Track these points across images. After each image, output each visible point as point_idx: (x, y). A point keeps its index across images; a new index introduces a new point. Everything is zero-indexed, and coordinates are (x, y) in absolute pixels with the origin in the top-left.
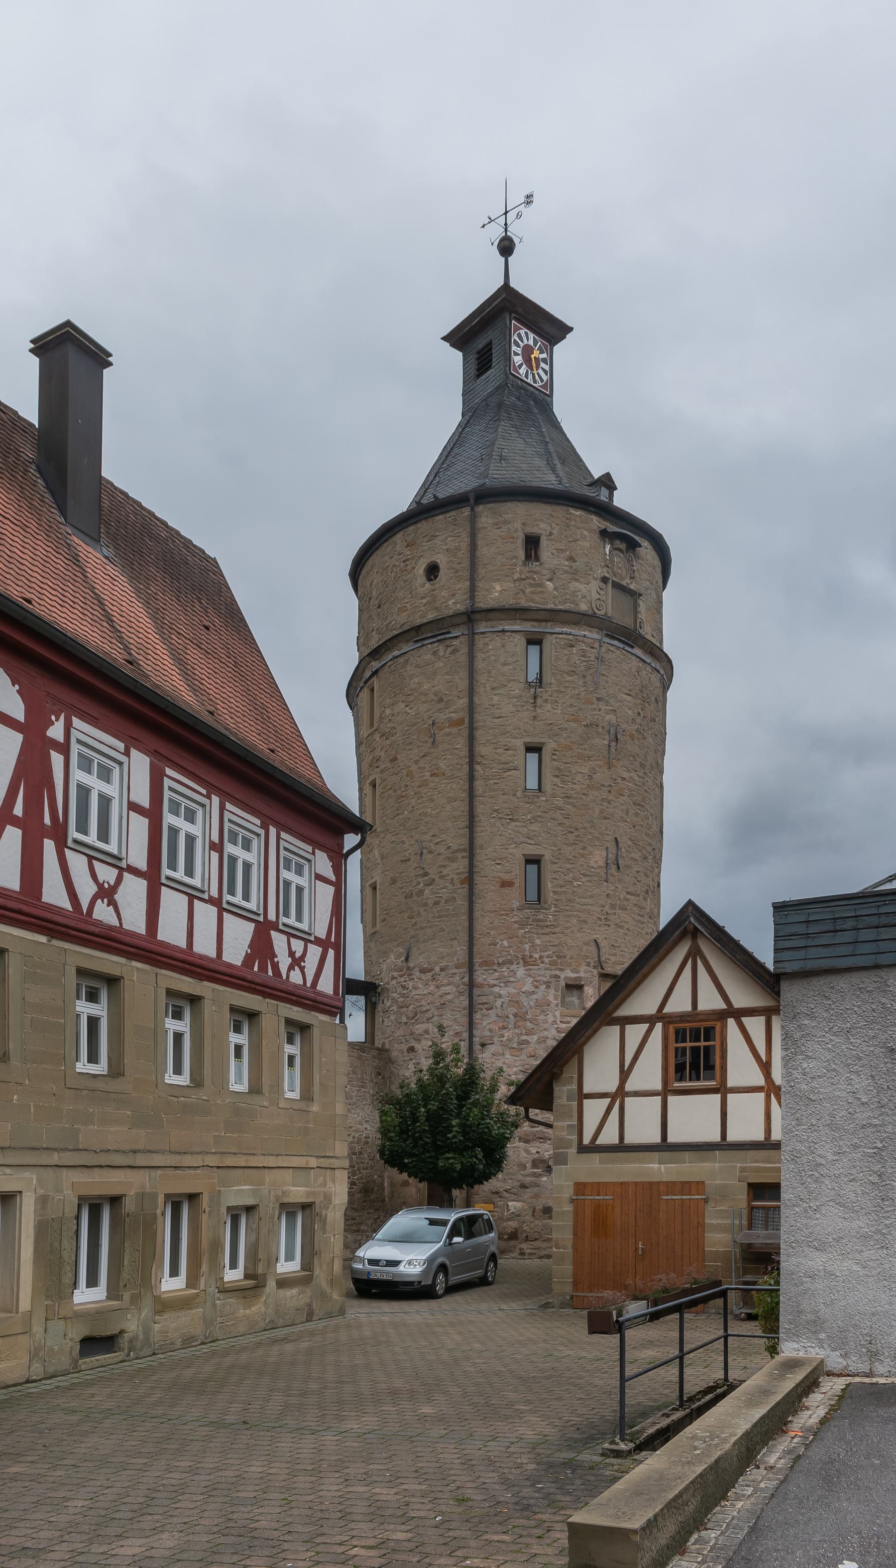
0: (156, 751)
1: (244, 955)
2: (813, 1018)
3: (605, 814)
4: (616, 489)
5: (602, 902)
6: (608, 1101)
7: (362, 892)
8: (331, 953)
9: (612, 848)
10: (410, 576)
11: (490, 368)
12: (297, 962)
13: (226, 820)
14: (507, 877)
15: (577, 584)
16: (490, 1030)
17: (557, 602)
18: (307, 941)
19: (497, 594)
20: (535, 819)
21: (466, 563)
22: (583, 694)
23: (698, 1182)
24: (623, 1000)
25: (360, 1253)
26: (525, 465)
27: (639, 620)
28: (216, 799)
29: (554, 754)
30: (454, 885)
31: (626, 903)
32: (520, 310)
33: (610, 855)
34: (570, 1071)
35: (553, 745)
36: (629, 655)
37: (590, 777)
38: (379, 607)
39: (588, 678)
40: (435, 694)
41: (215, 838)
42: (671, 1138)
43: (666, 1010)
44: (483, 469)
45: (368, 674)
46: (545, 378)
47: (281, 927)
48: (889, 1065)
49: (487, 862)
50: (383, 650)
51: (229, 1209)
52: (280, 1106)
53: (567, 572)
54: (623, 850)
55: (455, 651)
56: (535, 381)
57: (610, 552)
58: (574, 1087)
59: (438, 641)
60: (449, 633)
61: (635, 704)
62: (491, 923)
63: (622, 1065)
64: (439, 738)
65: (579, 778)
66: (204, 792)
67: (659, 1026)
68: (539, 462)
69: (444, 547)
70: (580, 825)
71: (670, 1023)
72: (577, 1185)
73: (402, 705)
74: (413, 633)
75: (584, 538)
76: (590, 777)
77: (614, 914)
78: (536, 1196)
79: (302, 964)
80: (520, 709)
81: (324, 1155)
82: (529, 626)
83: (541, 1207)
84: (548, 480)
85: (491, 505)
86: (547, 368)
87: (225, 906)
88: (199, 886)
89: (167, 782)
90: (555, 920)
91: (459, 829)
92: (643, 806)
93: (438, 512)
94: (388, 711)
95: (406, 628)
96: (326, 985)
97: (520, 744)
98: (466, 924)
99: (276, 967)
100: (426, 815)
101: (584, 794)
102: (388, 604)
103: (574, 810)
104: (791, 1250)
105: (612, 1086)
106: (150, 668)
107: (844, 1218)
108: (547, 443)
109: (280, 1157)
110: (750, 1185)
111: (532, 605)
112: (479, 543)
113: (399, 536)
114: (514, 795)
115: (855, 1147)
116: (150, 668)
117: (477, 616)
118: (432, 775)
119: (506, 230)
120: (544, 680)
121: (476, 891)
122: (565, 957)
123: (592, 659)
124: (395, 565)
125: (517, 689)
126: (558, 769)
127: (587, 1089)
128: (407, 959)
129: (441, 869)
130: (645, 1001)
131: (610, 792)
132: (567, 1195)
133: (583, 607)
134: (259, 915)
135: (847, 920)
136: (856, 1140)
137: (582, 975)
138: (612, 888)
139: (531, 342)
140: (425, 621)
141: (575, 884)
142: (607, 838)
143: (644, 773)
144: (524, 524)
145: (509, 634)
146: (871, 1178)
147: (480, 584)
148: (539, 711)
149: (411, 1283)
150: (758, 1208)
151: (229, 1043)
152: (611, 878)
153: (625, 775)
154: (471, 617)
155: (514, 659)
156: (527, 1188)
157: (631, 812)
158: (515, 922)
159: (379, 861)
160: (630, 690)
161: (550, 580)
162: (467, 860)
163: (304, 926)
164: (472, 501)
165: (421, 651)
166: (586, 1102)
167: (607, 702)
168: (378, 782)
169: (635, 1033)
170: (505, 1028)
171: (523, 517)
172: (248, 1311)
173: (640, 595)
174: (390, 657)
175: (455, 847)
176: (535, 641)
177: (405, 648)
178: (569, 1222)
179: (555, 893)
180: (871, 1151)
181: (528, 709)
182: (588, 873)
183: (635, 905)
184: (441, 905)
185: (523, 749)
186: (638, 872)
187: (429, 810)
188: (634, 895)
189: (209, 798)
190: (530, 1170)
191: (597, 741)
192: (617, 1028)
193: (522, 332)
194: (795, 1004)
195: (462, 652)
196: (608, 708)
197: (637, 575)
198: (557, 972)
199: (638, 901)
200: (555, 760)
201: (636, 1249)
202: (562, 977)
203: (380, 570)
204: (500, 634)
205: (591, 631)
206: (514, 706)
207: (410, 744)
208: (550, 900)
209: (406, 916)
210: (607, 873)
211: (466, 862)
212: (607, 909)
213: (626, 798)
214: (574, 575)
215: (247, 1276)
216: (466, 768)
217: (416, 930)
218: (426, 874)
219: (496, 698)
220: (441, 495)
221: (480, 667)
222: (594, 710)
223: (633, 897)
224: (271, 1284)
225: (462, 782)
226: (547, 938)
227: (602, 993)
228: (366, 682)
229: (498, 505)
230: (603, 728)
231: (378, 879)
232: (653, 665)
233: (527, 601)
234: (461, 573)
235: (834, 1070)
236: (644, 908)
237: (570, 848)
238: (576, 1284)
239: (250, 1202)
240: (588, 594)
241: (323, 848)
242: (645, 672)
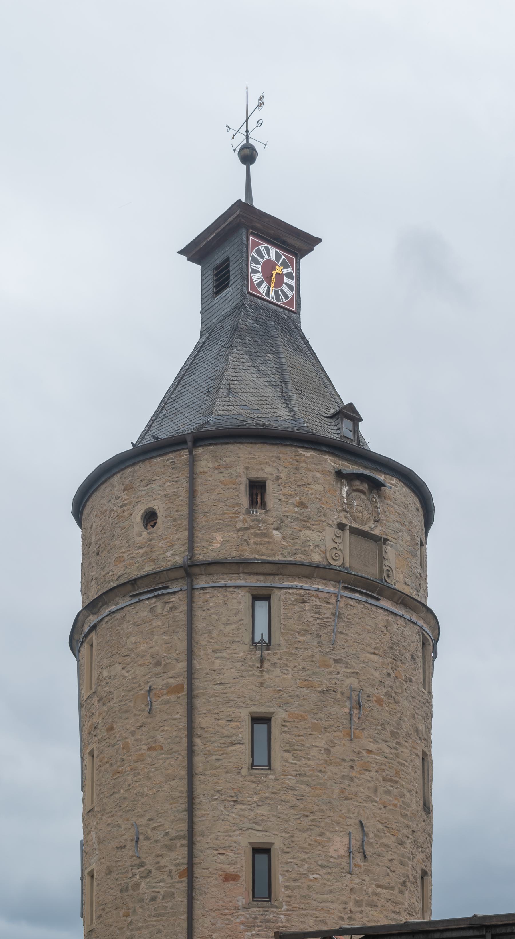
3: (346, 794)
4: (361, 420)
5: (344, 898)
7: (82, 880)
9: (357, 834)
10: (127, 523)
11: (227, 286)
14: (231, 870)
15: (308, 533)
17: (285, 552)
19: (218, 545)
20: (263, 801)
21: (185, 511)
22: (318, 656)
26: (256, 398)
27: (385, 568)
29: (284, 726)
30: (172, 878)
31: (375, 898)
32: (258, 225)
33: (354, 842)
36: (374, 609)
37: (328, 751)
38: (98, 554)
39: (324, 637)
40: (153, 657)
44: (209, 404)
45: (86, 629)
46: (290, 294)
49: (209, 852)
50: (100, 604)
53: (296, 519)
54: (371, 835)
55: (173, 608)
57: (348, 494)
59: (155, 596)
60: (166, 588)
61: (383, 664)
62: (213, 924)
64: (156, 706)
65: (314, 752)
68: (272, 395)
69: (162, 493)
70: (316, 808)
73: (119, 667)
74: (129, 587)
75: (316, 480)
76: (328, 751)
77: (361, 912)
80: (244, 674)
82: (254, 581)
84: (277, 415)
85: (212, 447)
86: (292, 283)
90: (288, 921)
91: (178, 812)
92: (396, 782)
93: (154, 454)
94: (105, 673)
95: (123, 580)
97: (245, 714)
98: (185, 925)
100: (142, 794)
101: (321, 771)
102: (105, 552)
103: (308, 789)
108: (284, 371)
111: (258, 557)
112: (199, 488)
113: (117, 478)
114: (239, 773)
117: (196, 570)
118: (149, 749)
119: (247, 137)
121: (196, 885)
123: (328, 615)
124: (113, 510)
125: (242, 650)
126: (289, 742)
129: (159, 859)
131: (352, 767)
133: (316, 558)
138: (357, 881)
139: (273, 258)
140: (142, 573)
141: (311, 877)
142: (350, 822)
143: (397, 743)
144: (247, 468)
145: (231, 589)
147: (199, 535)
148: (266, 676)
152: (356, 870)
153: (372, 746)
154: (190, 570)
155: (237, 618)
157: (381, 790)
158: (241, 923)
159: (96, 846)
160: (376, 649)
161: (277, 529)
162: (186, 849)
164: (190, 444)
165: (138, 608)
167: (347, 663)
168: (96, 752)
171: (246, 460)
173: (386, 540)
174: (107, 612)
175: (173, 833)
176: (261, 596)
177: (122, 604)
179: (287, 888)
181: (253, 675)
182: (327, 864)
183: (388, 900)
184: (159, 901)
185: (248, 722)
186: (391, 860)
187: (146, 789)
188: (386, 888)
191: (335, 709)
193: (262, 248)
195: (180, 610)
196: (349, 670)
197: (382, 517)
199: (392, 895)
200: (285, 732)
203: (99, 514)
204: (222, 590)
205: (326, 585)
206: (238, 671)
207: (127, 712)
209: (121, 912)
210: (349, 863)
211: (185, 851)
212: (351, 906)
213: (373, 774)
214: (306, 522)
216: (185, 741)
217: (132, 930)
218: (142, 865)
219: (218, 662)
220: (163, 436)
221: (200, 627)
222: (331, 673)
223: (385, 891)
225: (181, 757)
229: (219, 447)
230: (342, 693)
231: (94, 866)
232: (407, 616)
233: (251, 553)
234: (179, 522)
237: (305, 835)
240: (322, 543)
242: (396, 626)
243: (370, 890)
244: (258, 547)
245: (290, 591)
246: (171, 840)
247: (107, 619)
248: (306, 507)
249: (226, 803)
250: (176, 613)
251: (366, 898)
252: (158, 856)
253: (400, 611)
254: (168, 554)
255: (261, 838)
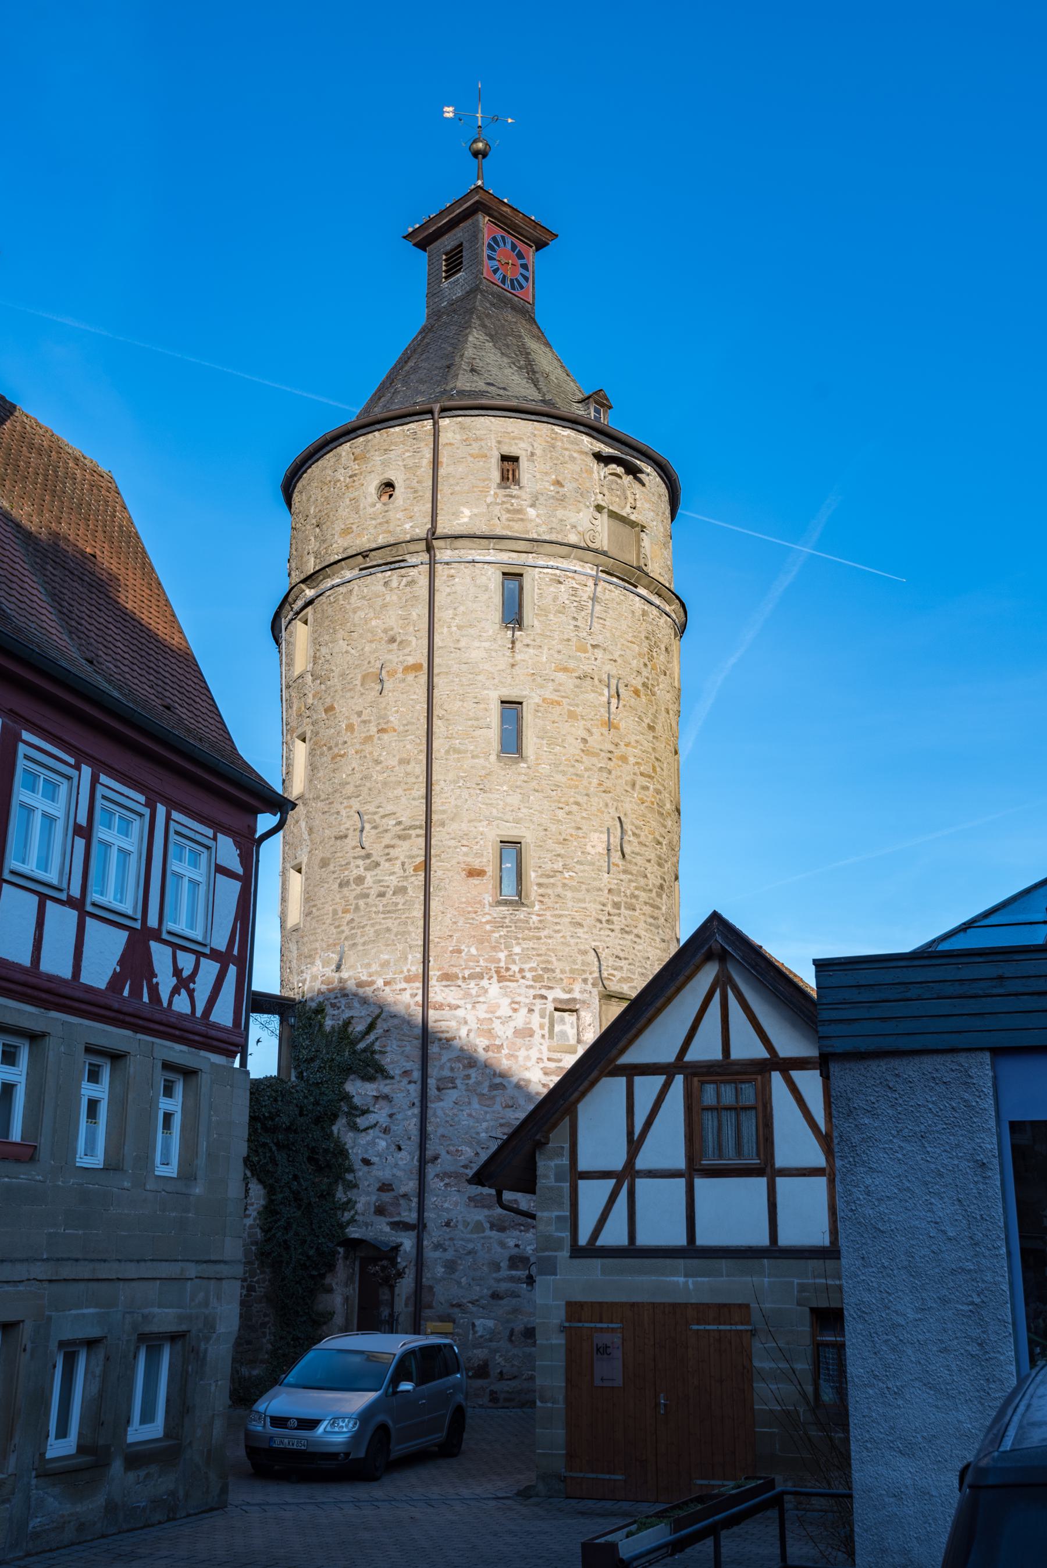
0: (11, 710)
1: (110, 973)
2: (875, 1116)
6: (612, 1182)
8: (232, 970)
12: (184, 983)
13: (98, 796)
14: (477, 864)
16: (452, 1069)
18: (199, 955)
19: (466, 520)
23: (740, 1306)
24: (631, 1042)
25: (261, 1406)
27: (642, 556)
28: (86, 771)
30: (405, 871)
31: (634, 901)
34: (558, 1138)
35: (537, 700)
41: (82, 820)
42: (701, 1240)
43: (688, 1058)
47: (165, 936)
48: (981, 1186)
50: (321, 577)
51: (62, 1344)
52: (148, 1187)
56: (513, 288)
58: (565, 1161)
63: (630, 1133)
65: (570, 739)
66: (72, 761)
67: (679, 1079)
71: (695, 1075)
72: (569, 1304)
78: (516, 1311)
79: (192, 986)
81: (207, 1258)
83: (521, 1327)
87: (89, 908)
88: (55, 882)
89: (22, 749)
96: (223, 1015)
97: (494, 697)
99: (154, 990)
104: (865, 1454)
105: (617, 1161)
106: (13, 606)
107: (937, 1407)
109: (142, 1264)
110: (813, 1310)
115: (944, 1301)
116: (13, 606)
120: (526, 621)
122: (553, 971)
127: (583, 1166)
128: (338, 968)
130: (658, 1044)
132: (557, 1321)
134: (135, 920)
135: (910, 986)
136: (945, 1292)
137: (577, 995)
141: (567, 875)
144: (499, 442)
146: (969, 1348)
149: (334, 1456)
150: (827, 1345)
151: (79, 1096)
156: (501, 1298)
158: (488, 922)
160: (634, 636)
161: (533, 506)
163: (197, 934)
166: (581, 1182)
169: (647, 1087)
170: (471, 1067)
172: (79, 1508)
177: (348, 575)
178: (559, 1361)
179: (540, 885)
180: (965, 1308)
189: (77, 767)
190: (505, 1273)
192: (622, 1081)
194: (851, 1096)
198: (543, 992)
199: (650, 898)
201: (657, 1404)
202: (550, 998)
206: (486, 650)
208: (533, 896)
211: (421, 841)
215: (81, 1449)
217: (353, 928)
218: (368, 856)
224: (117, 1466)
226: (531, 944)
227: (603, 1030)
228: (298, 613)
235: (908, 1189)
236: (658, 908)
238: (571, 1456)
239: (94, 1332)
240: (583, 523)
241: (228, 831)
243: (628, 892)
244: (511, 523)
245: (546, 571)
246: (404, 830)
247: (328, 593)
248: (562, 486)
249: (471, 791)
250: (416, 587)
251: (624, 899)
252: (387, 847)
253: (657, 601)
254: (407, 526)
255: (511, 832)
